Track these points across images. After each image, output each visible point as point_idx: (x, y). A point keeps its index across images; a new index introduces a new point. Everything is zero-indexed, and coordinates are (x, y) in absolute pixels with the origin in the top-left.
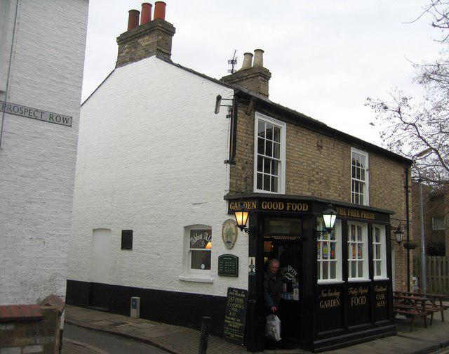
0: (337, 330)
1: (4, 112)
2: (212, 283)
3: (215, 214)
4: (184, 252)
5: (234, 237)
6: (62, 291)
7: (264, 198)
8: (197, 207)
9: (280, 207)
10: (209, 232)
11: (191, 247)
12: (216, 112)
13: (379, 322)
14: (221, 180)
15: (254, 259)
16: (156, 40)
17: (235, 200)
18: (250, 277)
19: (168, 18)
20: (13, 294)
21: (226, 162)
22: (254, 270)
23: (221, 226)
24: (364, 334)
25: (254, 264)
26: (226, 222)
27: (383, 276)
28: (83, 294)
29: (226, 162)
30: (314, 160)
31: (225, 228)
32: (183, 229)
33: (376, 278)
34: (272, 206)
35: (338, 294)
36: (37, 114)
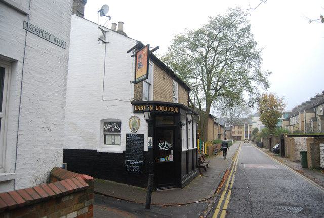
0: (233, 182)
1: (27, 30)
4: (100, 135)
5: (137, 126)
6: (60, 164)
8: (110, 108)
9: (165, 109)
10: (119, 123)
11: (104, 132)
14: (130, 93)
15: (152, 138)
16: (77, 5)
17: (138, 104)
20: (33, 169)
21: (132, 82)
22: (152, 145)
23: (129, 121)
25: (152, 141)
27: (195, 147)
29: (132, 82)
36: (47, 36)
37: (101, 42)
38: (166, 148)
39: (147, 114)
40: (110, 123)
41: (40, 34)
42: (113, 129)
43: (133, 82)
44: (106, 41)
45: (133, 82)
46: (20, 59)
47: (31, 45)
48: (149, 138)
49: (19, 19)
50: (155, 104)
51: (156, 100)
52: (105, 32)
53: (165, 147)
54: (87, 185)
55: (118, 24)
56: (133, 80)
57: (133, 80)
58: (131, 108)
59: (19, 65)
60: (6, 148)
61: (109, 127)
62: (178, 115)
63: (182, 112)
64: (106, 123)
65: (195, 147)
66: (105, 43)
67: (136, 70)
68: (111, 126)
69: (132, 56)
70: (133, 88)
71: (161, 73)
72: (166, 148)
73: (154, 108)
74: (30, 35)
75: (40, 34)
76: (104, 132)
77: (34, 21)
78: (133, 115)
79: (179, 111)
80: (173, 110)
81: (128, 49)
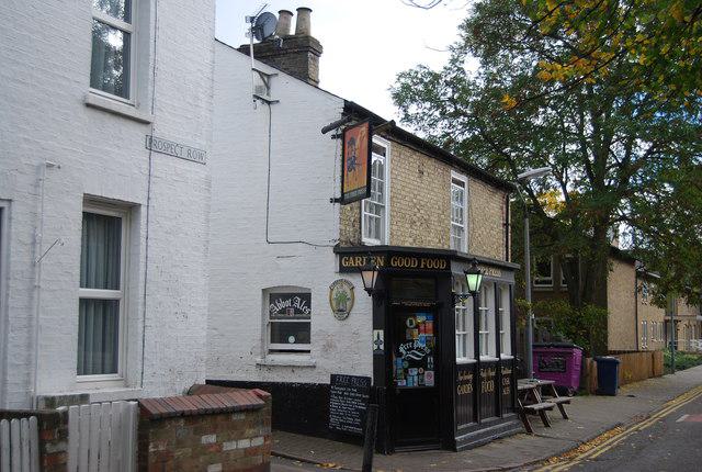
2: (315, 367)
3: (318, 274)
4: (263, 325)
7: (394, 252)
8: (281, 261)
9: (413, 264)
10: (306, 297)
12: (324, 131)
13: (464, 426)
14: (329, 225)
17: (351, 255)
18: (376, 357)
19: (315, 33)
22: (382, 347)
24: (488, 432)
25: (382, 338)
26: (336, 283)
27: (506, 355)
28: (208, 382)
30: (416, 192)
31: (334, 292)
32: (261, 293)
33: (503, 356)
34: (404, 263)
35: (470, 377)
37: (258, 102)
38: (418, 356)
39: (370, 277)
40: (285, 297)
41: (170, 150)
42: (292, 310)
43: (336, 200)
44: (271, 99)
45: (336, 200)
46: (143, 202)
47: (158, 174)
48: (376, 332)
49: (139, 132)
50: (389, 253)
51: (393, 244)
52: (268, 76)
53: (413, 354)
54: (262, 402)
55: (295, 13)
56: (338, 196)
57: (338, 196)
58: (332, 262)
59: (143, 210)
60: (127, 348)
61: (282, 305)
62: (447, 274)
63: (456, 269)
64: (272, 296)
65: (506, 355)
66: (269, 103)
67: (343, 171)
68: (288, 303)
69: (334, 137)
70: (337, 216)
71: (414, 159)
72: (418, 356)
73: (387, 262)
74: (157, 158)
75: (170, 150)
76: (86, 283)
77: (162, 130)
78: (338, 277)
79: (448, 267)
80: (433, 265)
81: (328, 124)
